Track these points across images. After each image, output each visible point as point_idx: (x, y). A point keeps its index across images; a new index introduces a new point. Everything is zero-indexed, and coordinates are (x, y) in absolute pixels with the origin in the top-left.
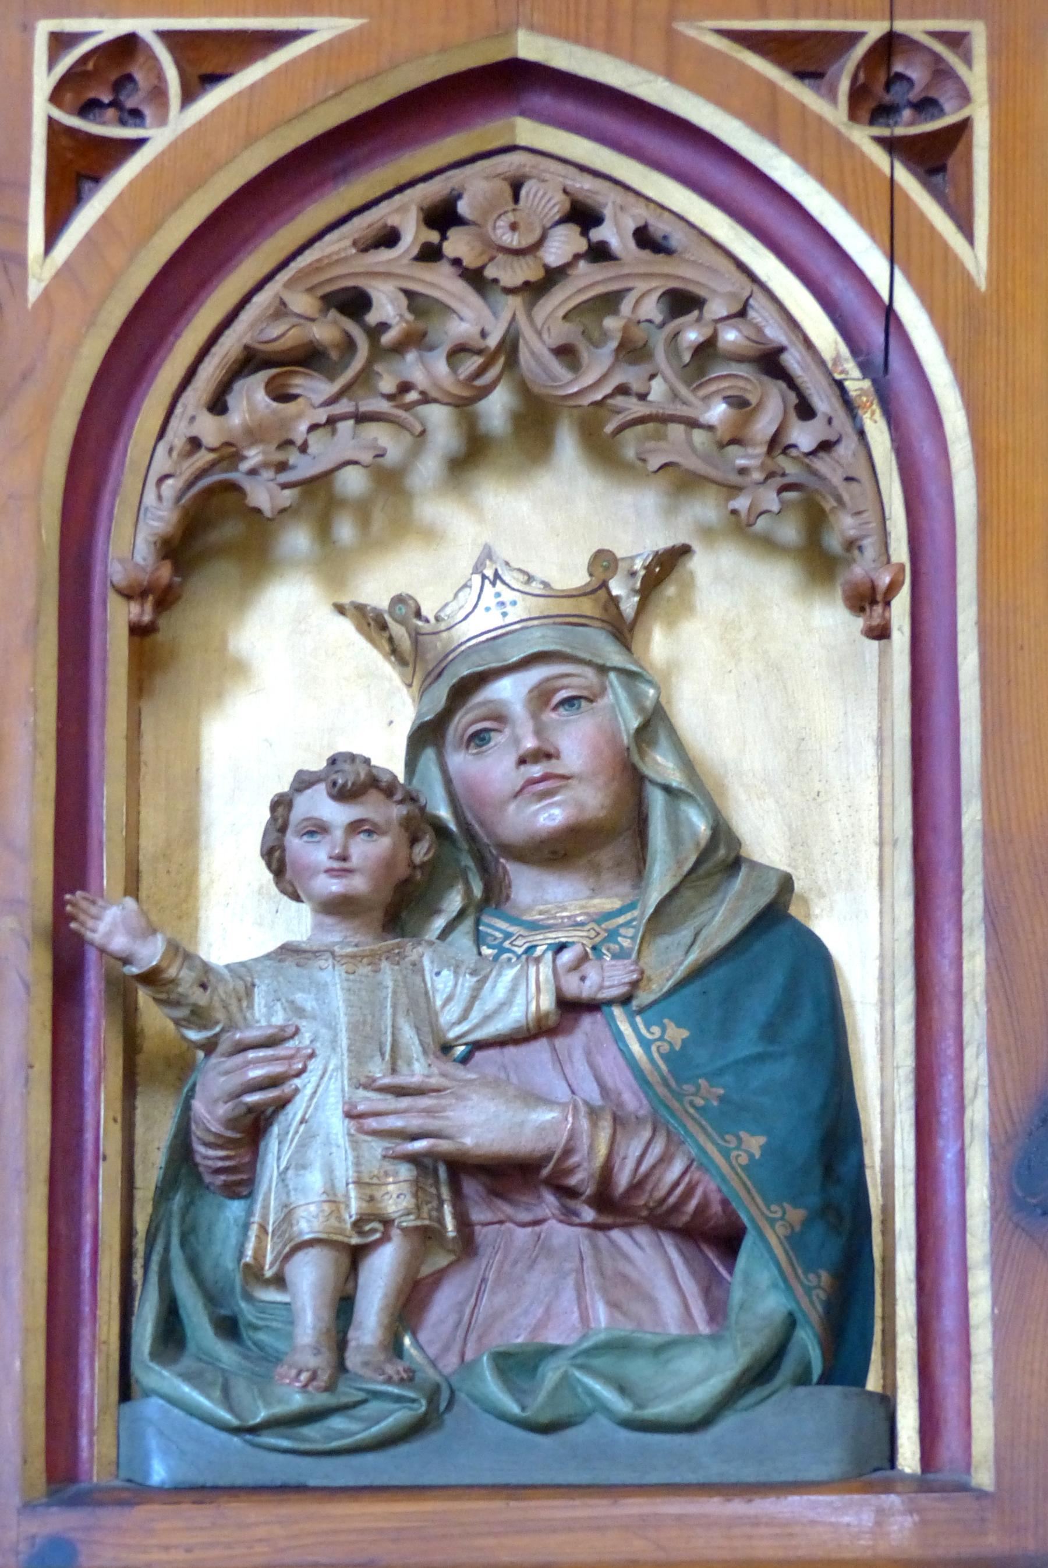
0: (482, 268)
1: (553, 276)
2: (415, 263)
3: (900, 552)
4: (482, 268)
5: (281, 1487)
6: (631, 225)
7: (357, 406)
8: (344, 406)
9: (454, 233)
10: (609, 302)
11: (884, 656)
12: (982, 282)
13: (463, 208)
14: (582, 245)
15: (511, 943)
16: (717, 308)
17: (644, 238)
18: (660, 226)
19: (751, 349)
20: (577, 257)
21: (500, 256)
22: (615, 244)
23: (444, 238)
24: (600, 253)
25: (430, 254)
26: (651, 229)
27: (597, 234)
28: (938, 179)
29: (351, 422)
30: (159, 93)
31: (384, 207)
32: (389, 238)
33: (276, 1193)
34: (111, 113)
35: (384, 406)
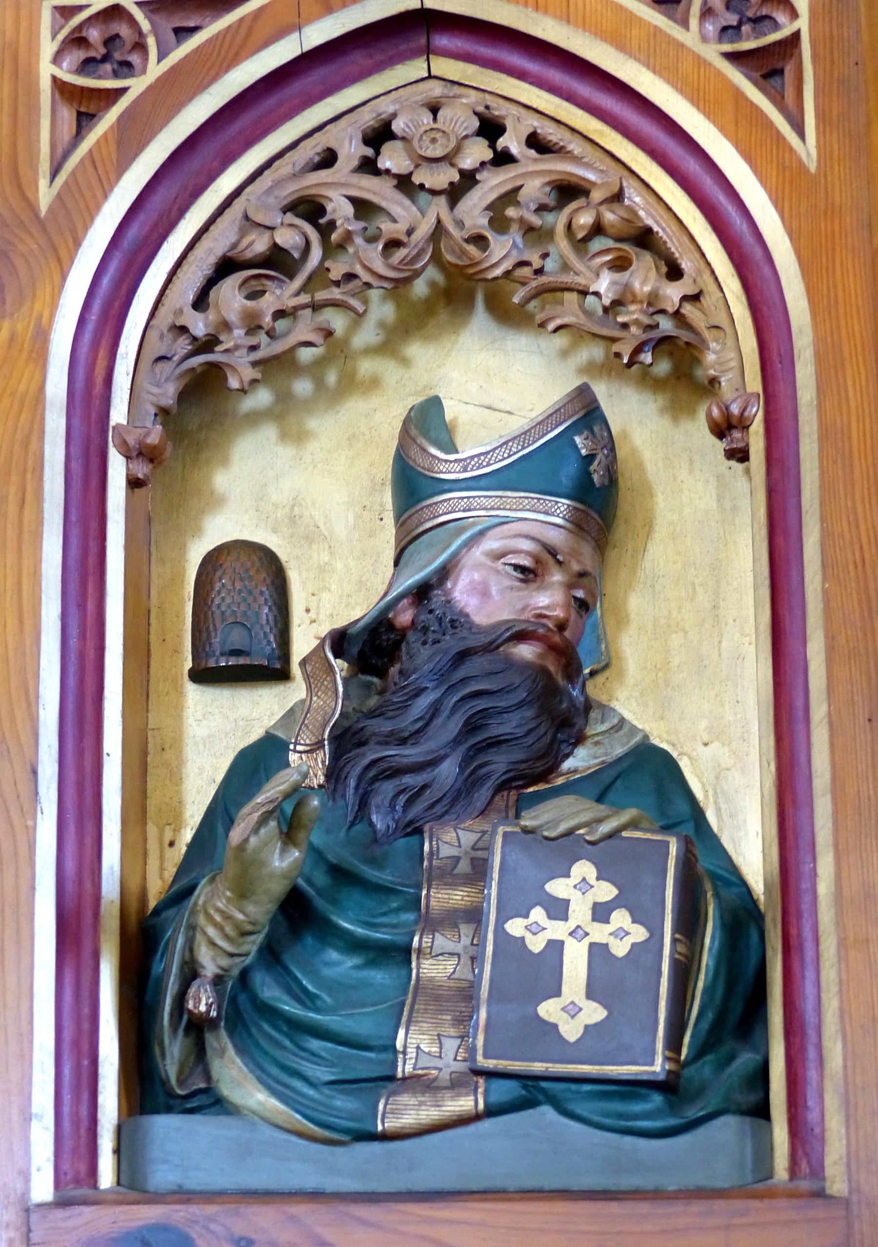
0: (411, 174)
1: (469, 179)
2: (354, 174)
3: (754, 384)
4: (411, 174)
5: (312, 1193)
6: (525, 132)
7: (312, 298)
8: (304, 298)
9: (387, 148)
10: (511, 197)
11: (748, 471)
12: (813, 168)
13: (397, 126)
14: (489, 155)
15: (437, 859)
16: (597, 195)
17: (534, 142)
18: (551, 133)
19: (627, 230)
20: (483, 164)
21: (424, 164)
22: (515, 150)
23: (378, 153)
24: (503, 159)
25: (368, 166)
26: (788, 19)
27: (501, 143)
28: (776, 81)
29: (310, 310)
30: (140, 46)
31: (514, 110)
32: (329, 159)
33: (449, 546)
34: (108, 67)
35: (335, 293)
